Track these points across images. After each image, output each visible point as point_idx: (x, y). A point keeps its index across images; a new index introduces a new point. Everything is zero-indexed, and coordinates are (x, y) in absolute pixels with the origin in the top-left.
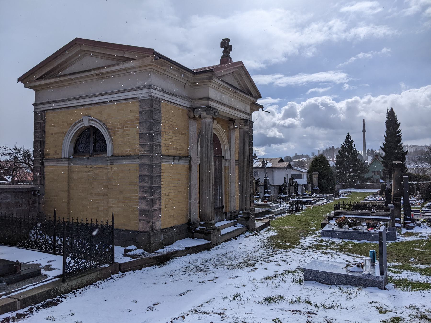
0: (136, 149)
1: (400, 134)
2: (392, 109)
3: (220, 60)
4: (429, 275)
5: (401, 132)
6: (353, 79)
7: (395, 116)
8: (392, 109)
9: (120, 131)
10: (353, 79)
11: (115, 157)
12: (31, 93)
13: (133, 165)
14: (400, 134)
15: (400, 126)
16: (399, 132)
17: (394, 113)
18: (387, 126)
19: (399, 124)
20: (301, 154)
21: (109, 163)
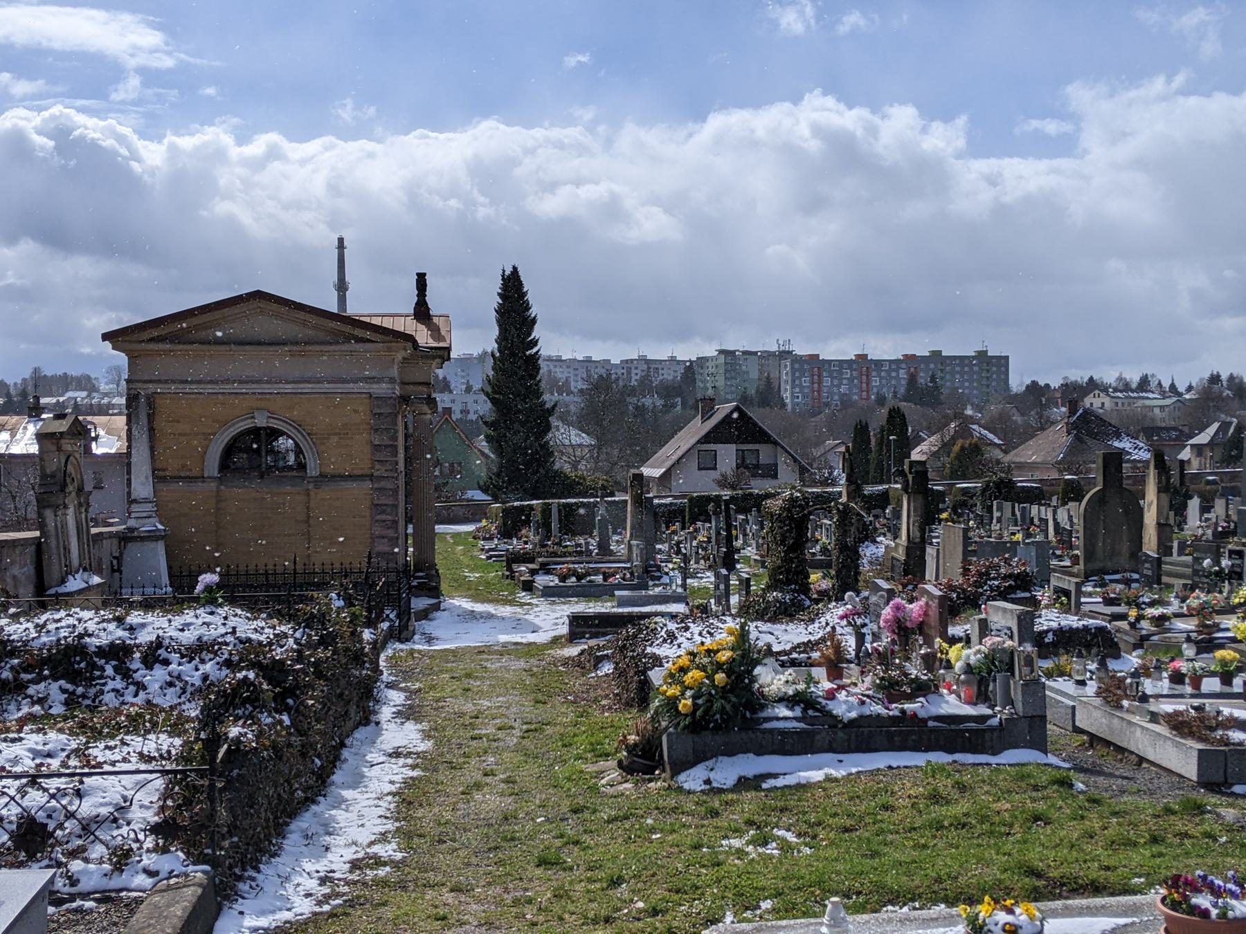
0: (363, 466)
1: (535, 350)
2: (515, 268)
3: (498, 321)
4: (1235, 576)
5: (539, 344)
6: (191, 60)
7: (525, 294)
8: (515, 268)
9: (335, 439)
10: (191, 60)
11: (325, 478)
12: (122, 359)
13: (360, 491)
14: (535, 350)
15: (536, 327)
16: (534, 343)
17: (521, 284)
18: (501, 323)
19: (534, 321)
20: (60, 373)
21: (311, 486)
